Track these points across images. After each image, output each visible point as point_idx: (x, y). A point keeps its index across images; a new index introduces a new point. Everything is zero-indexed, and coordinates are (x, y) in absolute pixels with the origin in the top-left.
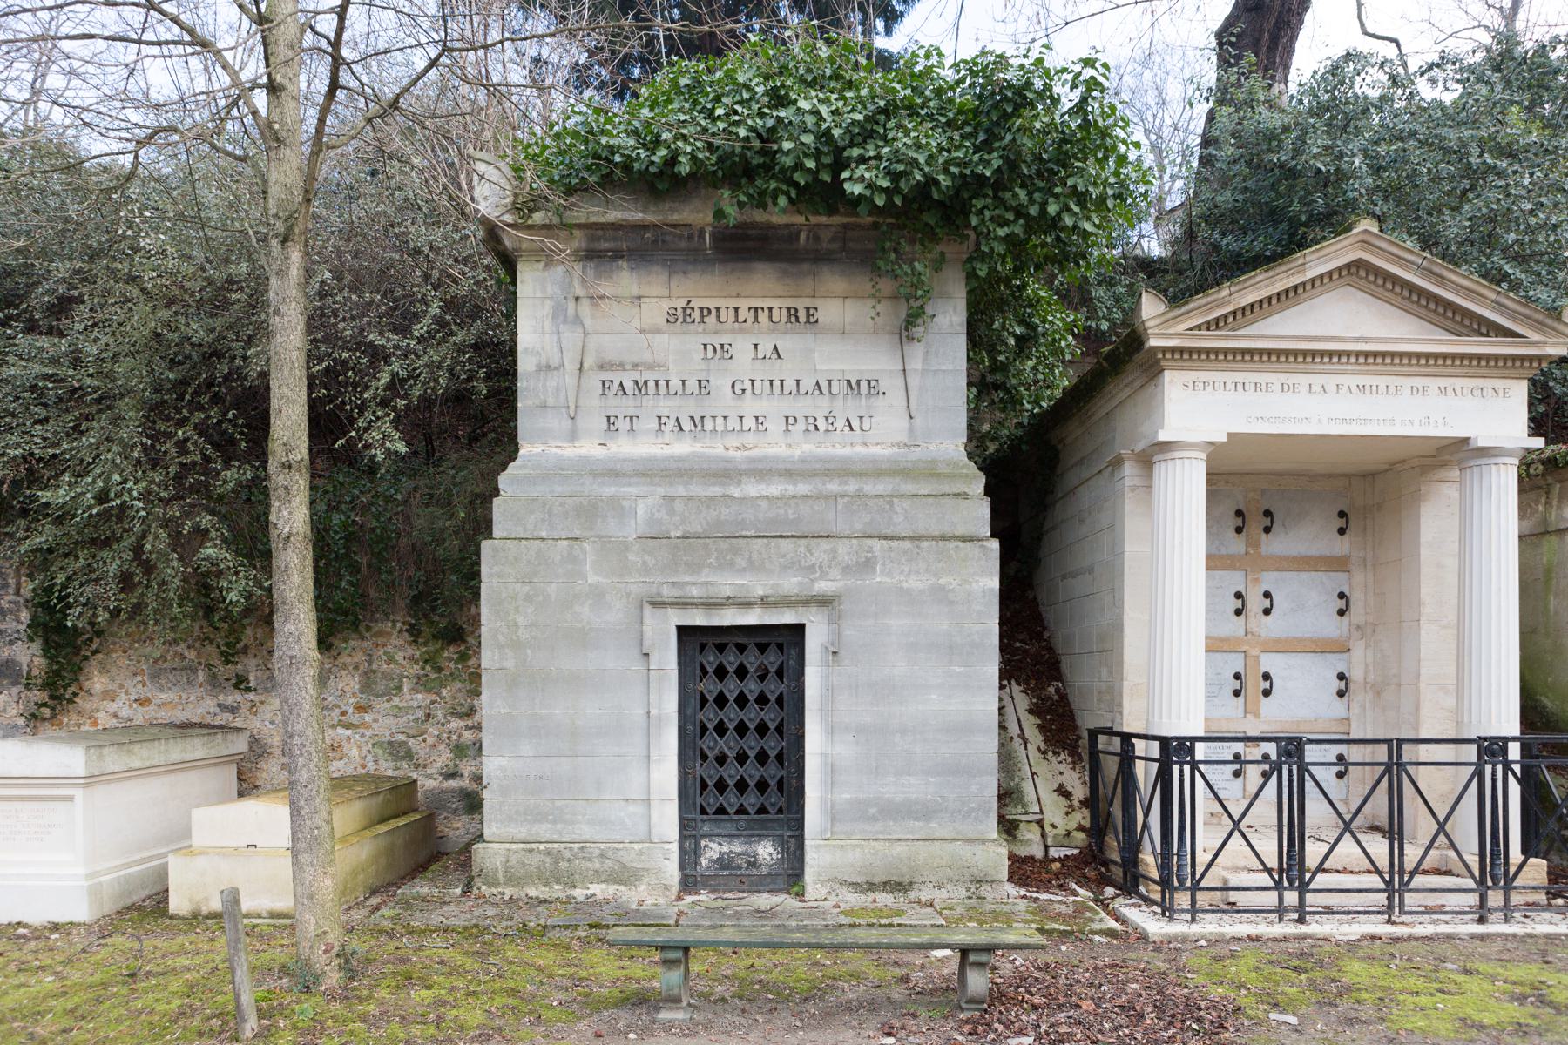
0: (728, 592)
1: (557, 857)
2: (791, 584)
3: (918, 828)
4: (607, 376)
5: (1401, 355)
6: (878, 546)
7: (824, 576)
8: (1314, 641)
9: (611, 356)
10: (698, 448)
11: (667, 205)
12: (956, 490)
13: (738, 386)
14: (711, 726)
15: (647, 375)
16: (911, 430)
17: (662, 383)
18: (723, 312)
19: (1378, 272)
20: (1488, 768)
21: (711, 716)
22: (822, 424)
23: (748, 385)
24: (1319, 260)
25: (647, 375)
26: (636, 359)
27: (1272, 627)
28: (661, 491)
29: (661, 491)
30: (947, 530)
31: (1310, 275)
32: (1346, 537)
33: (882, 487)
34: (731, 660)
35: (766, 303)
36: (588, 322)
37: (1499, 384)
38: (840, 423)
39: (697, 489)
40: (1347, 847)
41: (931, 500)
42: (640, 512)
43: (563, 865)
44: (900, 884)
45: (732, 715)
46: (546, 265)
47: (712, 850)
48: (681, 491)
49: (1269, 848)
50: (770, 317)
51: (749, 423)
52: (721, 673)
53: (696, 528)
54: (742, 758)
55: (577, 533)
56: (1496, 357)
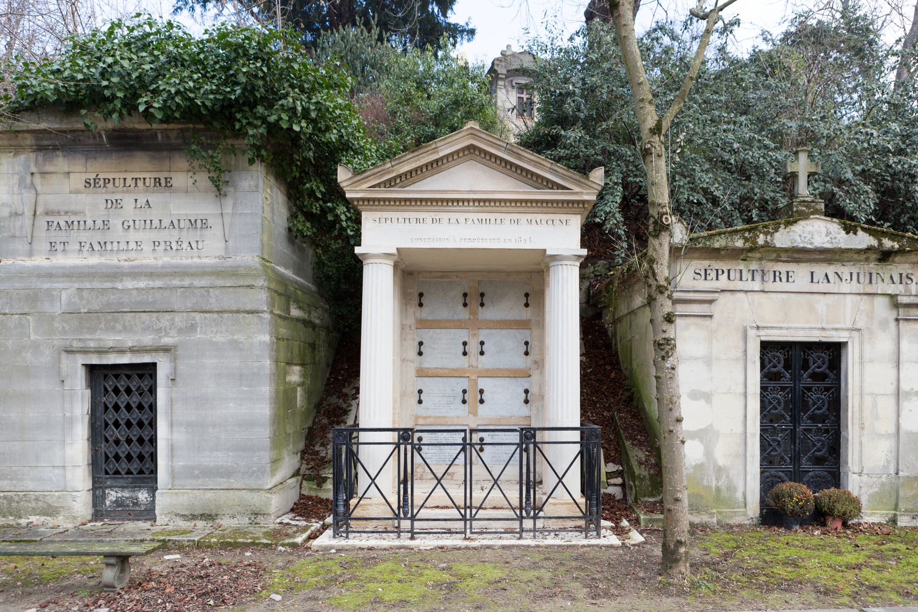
0: (111, 344)
1: (10, 500)
2: (148, 339)
3: (224, 482)
4: (50, 219)
5: (500, 201)
6: (198, 316)
7: (167, 335)
9: (53, 207)
10: (102, 260)
11: (74, 119)
12: (247, 284)
13: (126, 224)
14: (110, 423)
15: (74, 218)
16: (226, 248)
17: (82, 223)
18: (117, 181)
19: (481, 151)
21: (111, 416)
22: (174, 246)
23: (131, 223)
24: (446, 146)
25: (74, 218)
26: (67, 209)
27: (485, 362)
28: (76, 285)
29: (76, 285)
30: (241, 307)
31: (441, 154)
32: (529, 309)
33: (204, 282)
34: (122, 385)
35: (142, 175)
36: (39, 188)
37: (564, 217)
38: (185, 245)
39: (97, 285)
41: (231, 289)
42: (63, 298)
43: (14, 505)
44: (210, 515)
45: (124, 415)
46: (15, 155)
47: (112, 495)
48: (88, 285)
49: (514, 495)
50: (114, 184)
51: (132, 245)
52: (116, 391)
53: (96, 307)
54: (129, 441)
55: (27, 310)
56: (557, 202)
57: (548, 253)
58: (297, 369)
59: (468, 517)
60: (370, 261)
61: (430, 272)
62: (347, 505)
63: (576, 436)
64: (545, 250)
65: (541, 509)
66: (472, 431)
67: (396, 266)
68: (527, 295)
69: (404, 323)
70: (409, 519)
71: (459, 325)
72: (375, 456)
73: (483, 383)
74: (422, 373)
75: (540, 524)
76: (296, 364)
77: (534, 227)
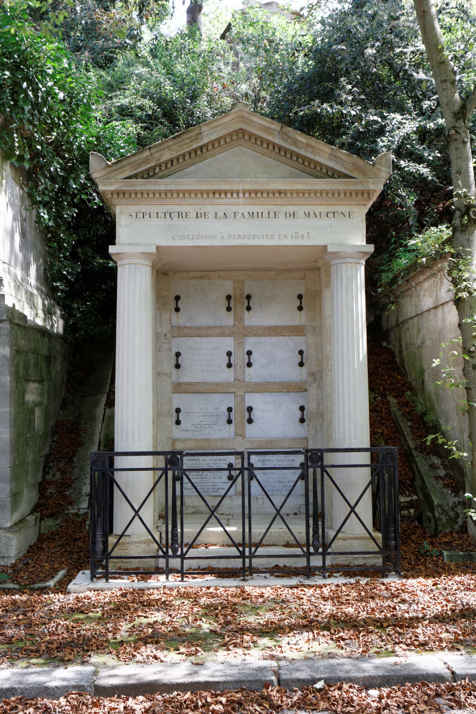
8: (281, 384)
20: (311, 471)
32: (303, 312)
40: (278, 529)
57: (330, 249)
58: (33, 386)
59: (247, 554)
60: (126, 261)
61: (188, 272)
62: (105, 543)
63: (365, 458)
64: (325, 247)
65: (330, 546)
66: (250, 454)
67: (153, 267)
68: (300, 297)
69: (158, 331)
70: (178, 557)
71: (222, 332)
72: (136, 483)
73: (253, 400)
74: (179, 388)
75: (329, 561)
76: (34, 381)
77: (312, 221)
